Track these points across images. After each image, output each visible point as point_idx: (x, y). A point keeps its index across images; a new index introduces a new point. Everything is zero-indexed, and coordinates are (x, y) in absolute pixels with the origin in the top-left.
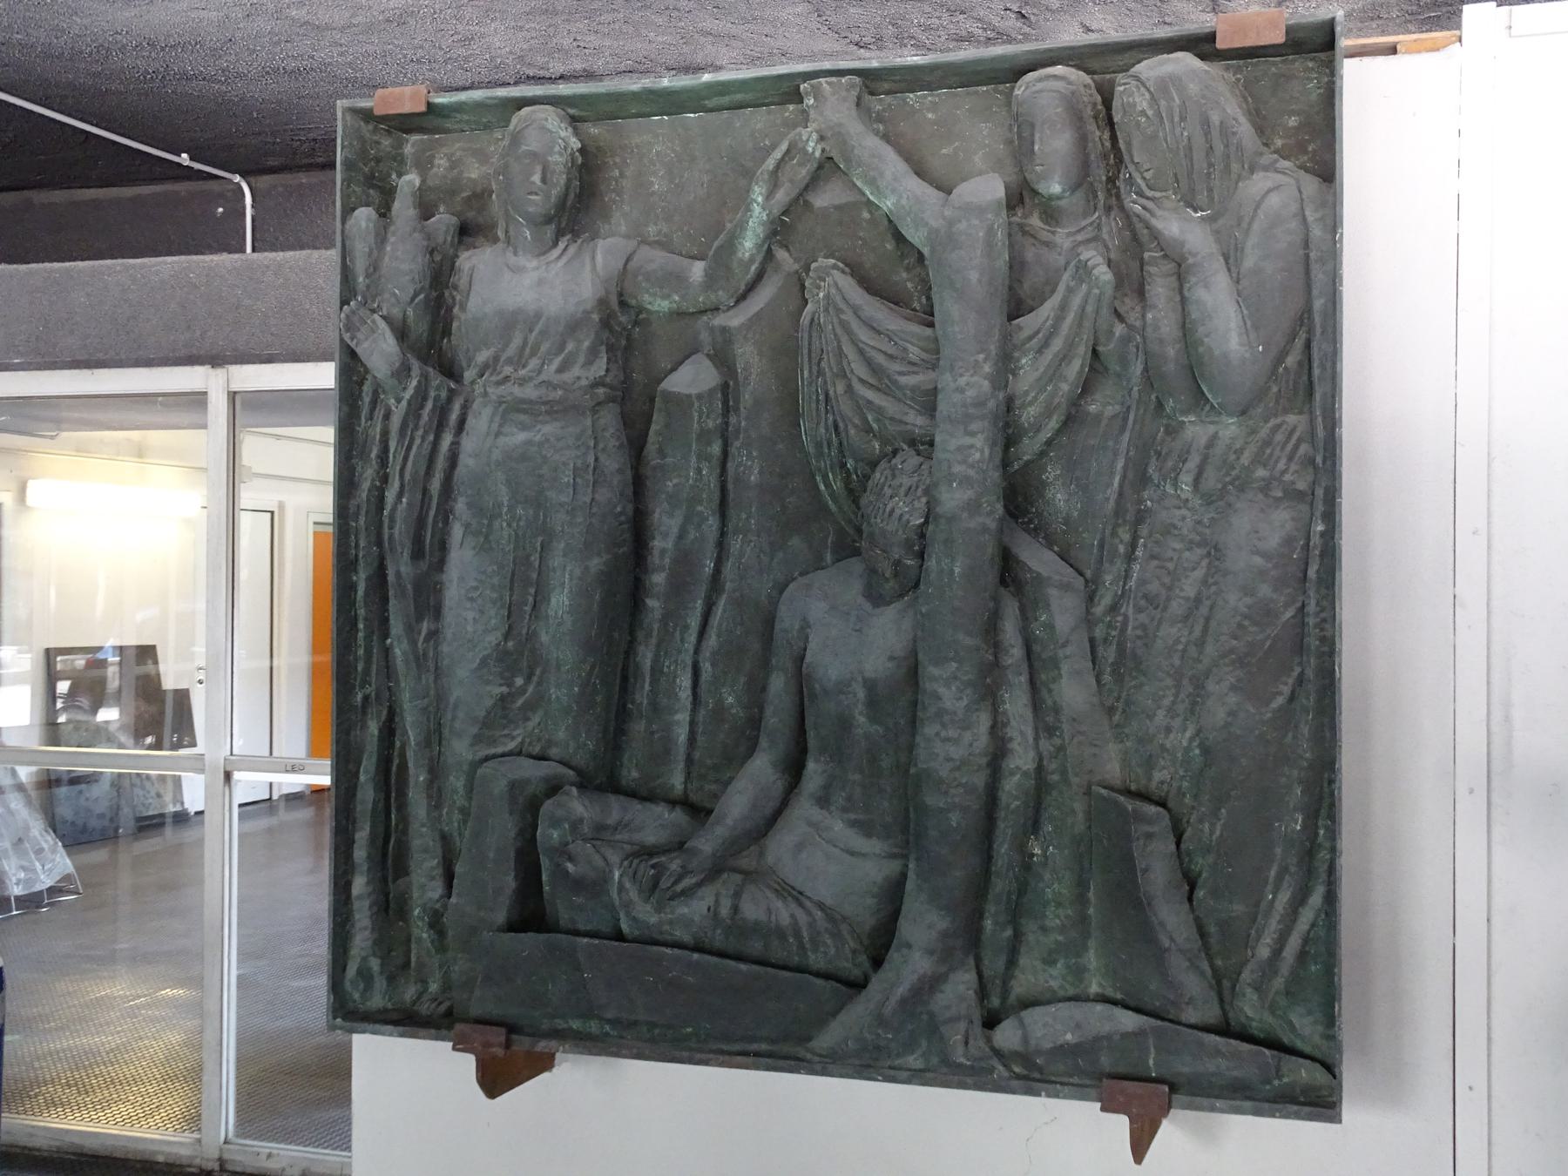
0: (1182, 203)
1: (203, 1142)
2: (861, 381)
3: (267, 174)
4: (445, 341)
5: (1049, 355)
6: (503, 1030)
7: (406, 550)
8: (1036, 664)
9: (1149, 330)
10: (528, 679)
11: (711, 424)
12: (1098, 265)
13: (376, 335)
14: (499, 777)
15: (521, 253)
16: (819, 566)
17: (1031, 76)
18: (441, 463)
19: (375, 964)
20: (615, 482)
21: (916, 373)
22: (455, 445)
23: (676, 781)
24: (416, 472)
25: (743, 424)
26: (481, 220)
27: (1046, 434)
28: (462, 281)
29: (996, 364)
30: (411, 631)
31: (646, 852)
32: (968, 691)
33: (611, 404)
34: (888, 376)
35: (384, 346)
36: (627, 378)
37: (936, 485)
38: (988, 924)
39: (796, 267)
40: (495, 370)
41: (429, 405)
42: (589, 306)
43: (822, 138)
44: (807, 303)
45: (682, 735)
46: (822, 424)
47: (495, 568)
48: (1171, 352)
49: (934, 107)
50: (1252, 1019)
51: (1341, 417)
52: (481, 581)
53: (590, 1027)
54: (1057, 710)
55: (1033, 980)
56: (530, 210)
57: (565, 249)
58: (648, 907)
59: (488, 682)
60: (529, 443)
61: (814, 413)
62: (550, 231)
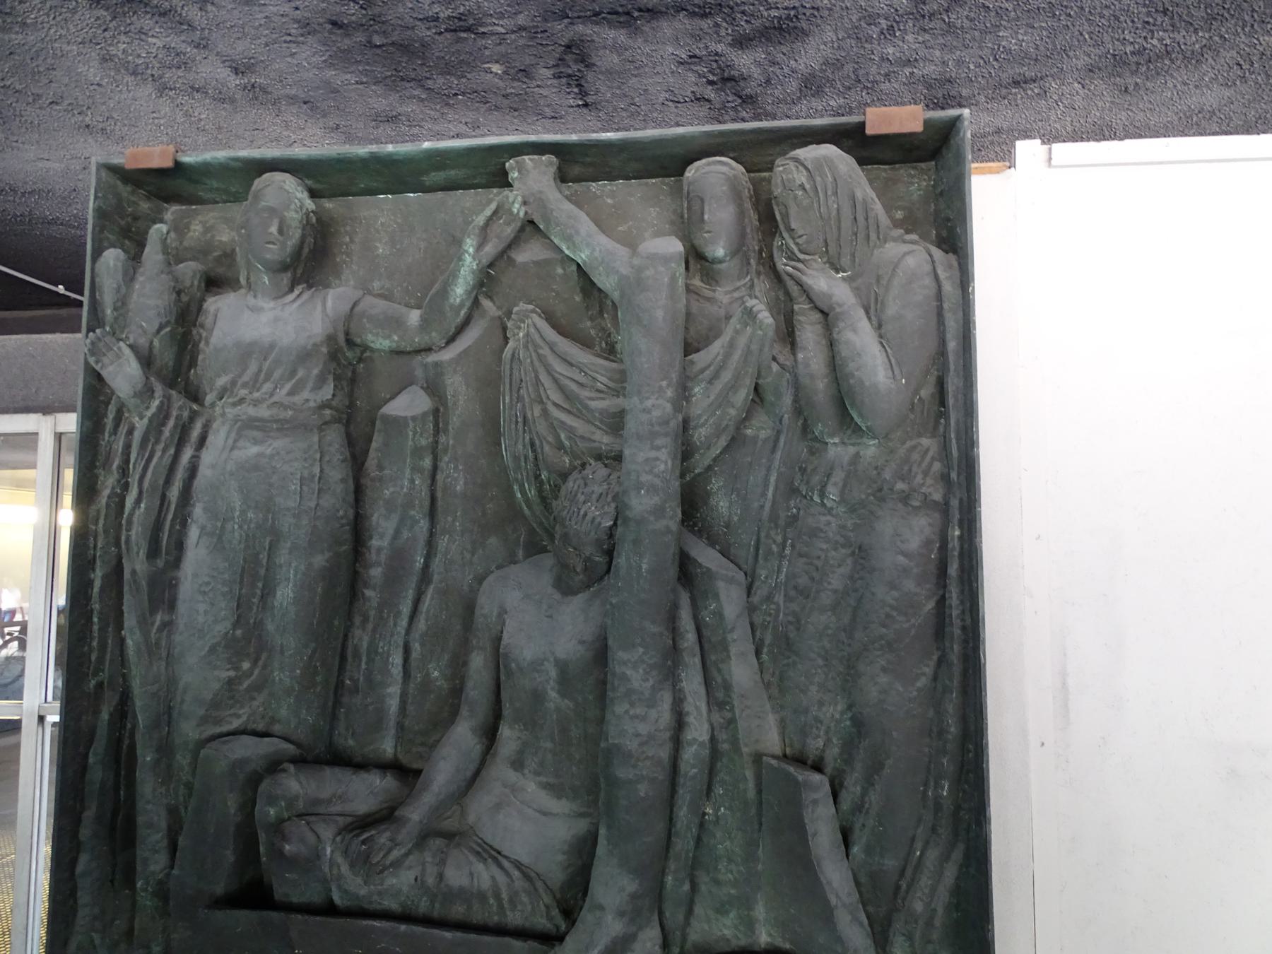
0: (827, 265)
4: (192, 371)
5: (718, 386)
7: (142, 551)
8: (706, 646)
9: (801, 367)
13: (121, 360)
15: (260, 296)
16: (514, 561)
18: (180, 475)
20: (338, 490)
21: (603, 399)
23: (387, 747)
25: (451, 442)
28: (208, 321)
29: (676, 391)
30: (144, 623)
34: (581, 403)
35: (129, 369)
37: (625, 492)
38: (669, 879)
39: (500, 313)
40: (232, 392)
41: (171, 423)
42: (319, 339)
43: (525, 203)
44: (507, 343)
45: (393, 705)
46: (520, 441)
47: (227, 564)
49: (612, 194)
52: (213, 577)
54: (727, 687)
57: (299, 296)
61: (514, 434)
62: (286, 278)
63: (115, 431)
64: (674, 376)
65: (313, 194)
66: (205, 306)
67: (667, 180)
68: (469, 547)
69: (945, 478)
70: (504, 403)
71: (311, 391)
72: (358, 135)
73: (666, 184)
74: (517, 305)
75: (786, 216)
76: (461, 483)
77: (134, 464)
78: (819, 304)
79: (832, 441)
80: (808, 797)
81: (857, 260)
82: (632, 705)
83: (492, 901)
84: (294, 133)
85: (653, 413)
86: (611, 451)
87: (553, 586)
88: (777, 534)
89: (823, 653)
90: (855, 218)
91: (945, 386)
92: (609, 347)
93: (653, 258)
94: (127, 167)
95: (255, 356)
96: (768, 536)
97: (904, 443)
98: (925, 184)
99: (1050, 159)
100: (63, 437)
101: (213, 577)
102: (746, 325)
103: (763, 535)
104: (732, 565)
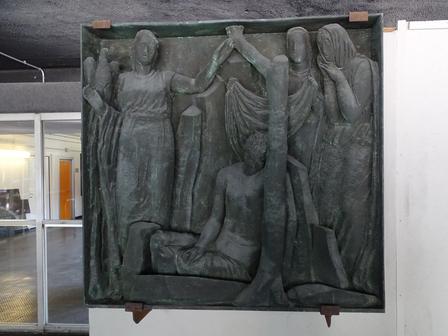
0: (335, 65)
1: (38, 325)
2: (244, 112)
3: (49, 68)
4: (115, 100)
5: (300, 106)
6: (141, 304)
8: (295, 191)
9: (326, 100)
10: (145, 198)
11: (198, 125)
12: (314, 81)
13: (94, 96)
14: (138, 228)
16: (228, 165)
17: (292, 29)
18: (115, 136)
19: (98, 286)
22: (120, 130)
25: (208, 125)
26: (125, 65)
27: (298, 128)
30: (107, 186)
31: (184, 249)
32: (279, 199)
33: (168, 119)
35: (97, 100)
36: (172, 112)
39: (223, 80)
40: (133, 107)
41: (112, 118)
42: (162, 89)
43: (234, 43)
45: (189, 213)
46: (232, 125)
48: (333, 106)
49: (261, 38)
50: (356, 285)
51: (383, 123)
53: (169, 301)
54: (302, 204)
56: (144, 60)
57: (153, 73)
58: (186, 265)
59: (132, 200)
60: (144, 129)
63: (93, 121)
64: (285, 103)
65: (157, 37)
66: (119, 77)
67: (280, 33)
69: (373, 136)
70: (226, 112)
71: (160, 107)
72: (154, 7)
73: (280, 35)
74: (230, 78)
75: (322, 48)
77: (101, 132)
78: (332, 78)
79: (336, 124)
80: (328, 236)
81: (345, 64)
82: (273, 209)
83: (228, 271)
84: (129, 5)
85: (279, 115)
87: (243, 173)
88: (318, 155)
89: (332, 193)
90: (345, 49)
91: (373, 106)
92: (260, 92)
93: (279, 63)
94: (94, 28)
95: (140, 95)
96: (315, 156)
97: (359, 124)
98: (367, 36)
99: (409, 27)
100: (43, 122)
101: (129, 170)
102: (309, 85)
103: (313, 155)
104: (303, 165)
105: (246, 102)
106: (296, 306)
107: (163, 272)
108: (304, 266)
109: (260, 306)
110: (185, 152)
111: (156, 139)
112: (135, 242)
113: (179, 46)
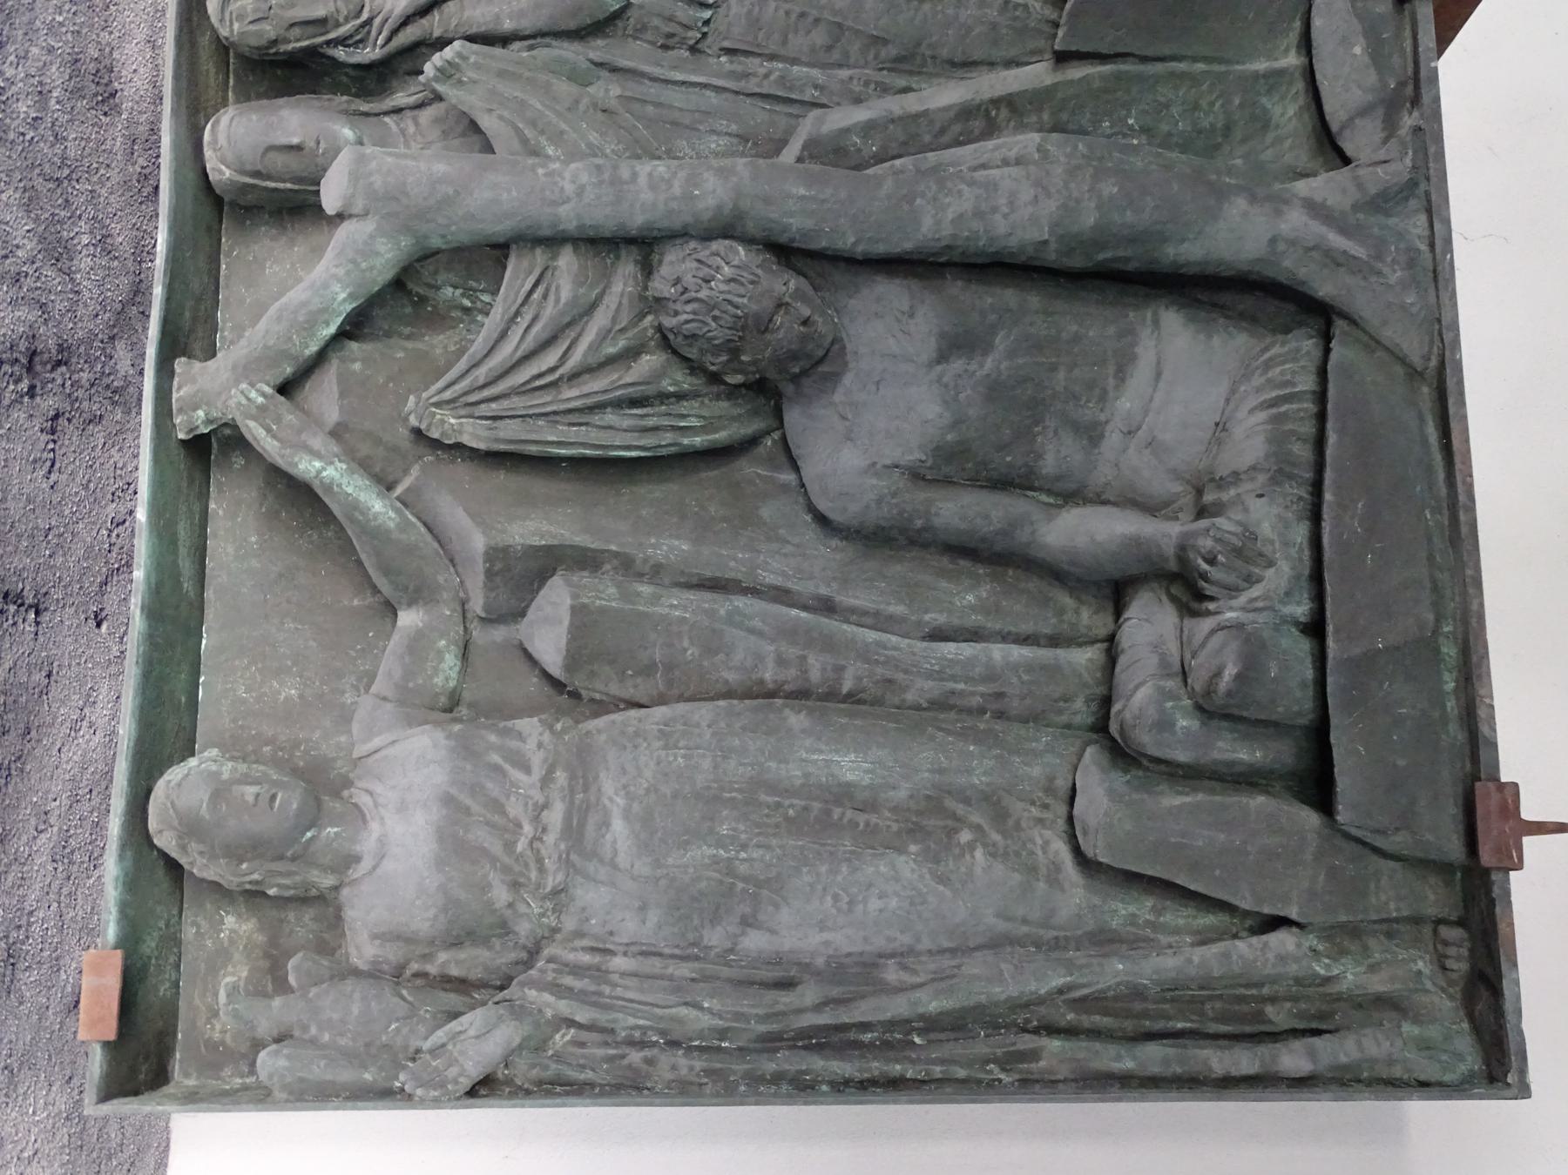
21: (558, 288)
24: (665, 989)
28: (391, 957)
45: (1019, 652)
55: (1290, 140)
56: (295, 806)
60: (627, 815)
68: (775, 546)
76: (677, 543)
82: (995, 210)
86: (635, 277)
101: (824, 889)
105: (517, 348)
106: (1416, 101)
107: (1311, 688)
108: (1237, 101)
109: (1432, 246)
110: (738, 657)
111: (676, 759)
112: (1173, 840)
113: (241, 692)
